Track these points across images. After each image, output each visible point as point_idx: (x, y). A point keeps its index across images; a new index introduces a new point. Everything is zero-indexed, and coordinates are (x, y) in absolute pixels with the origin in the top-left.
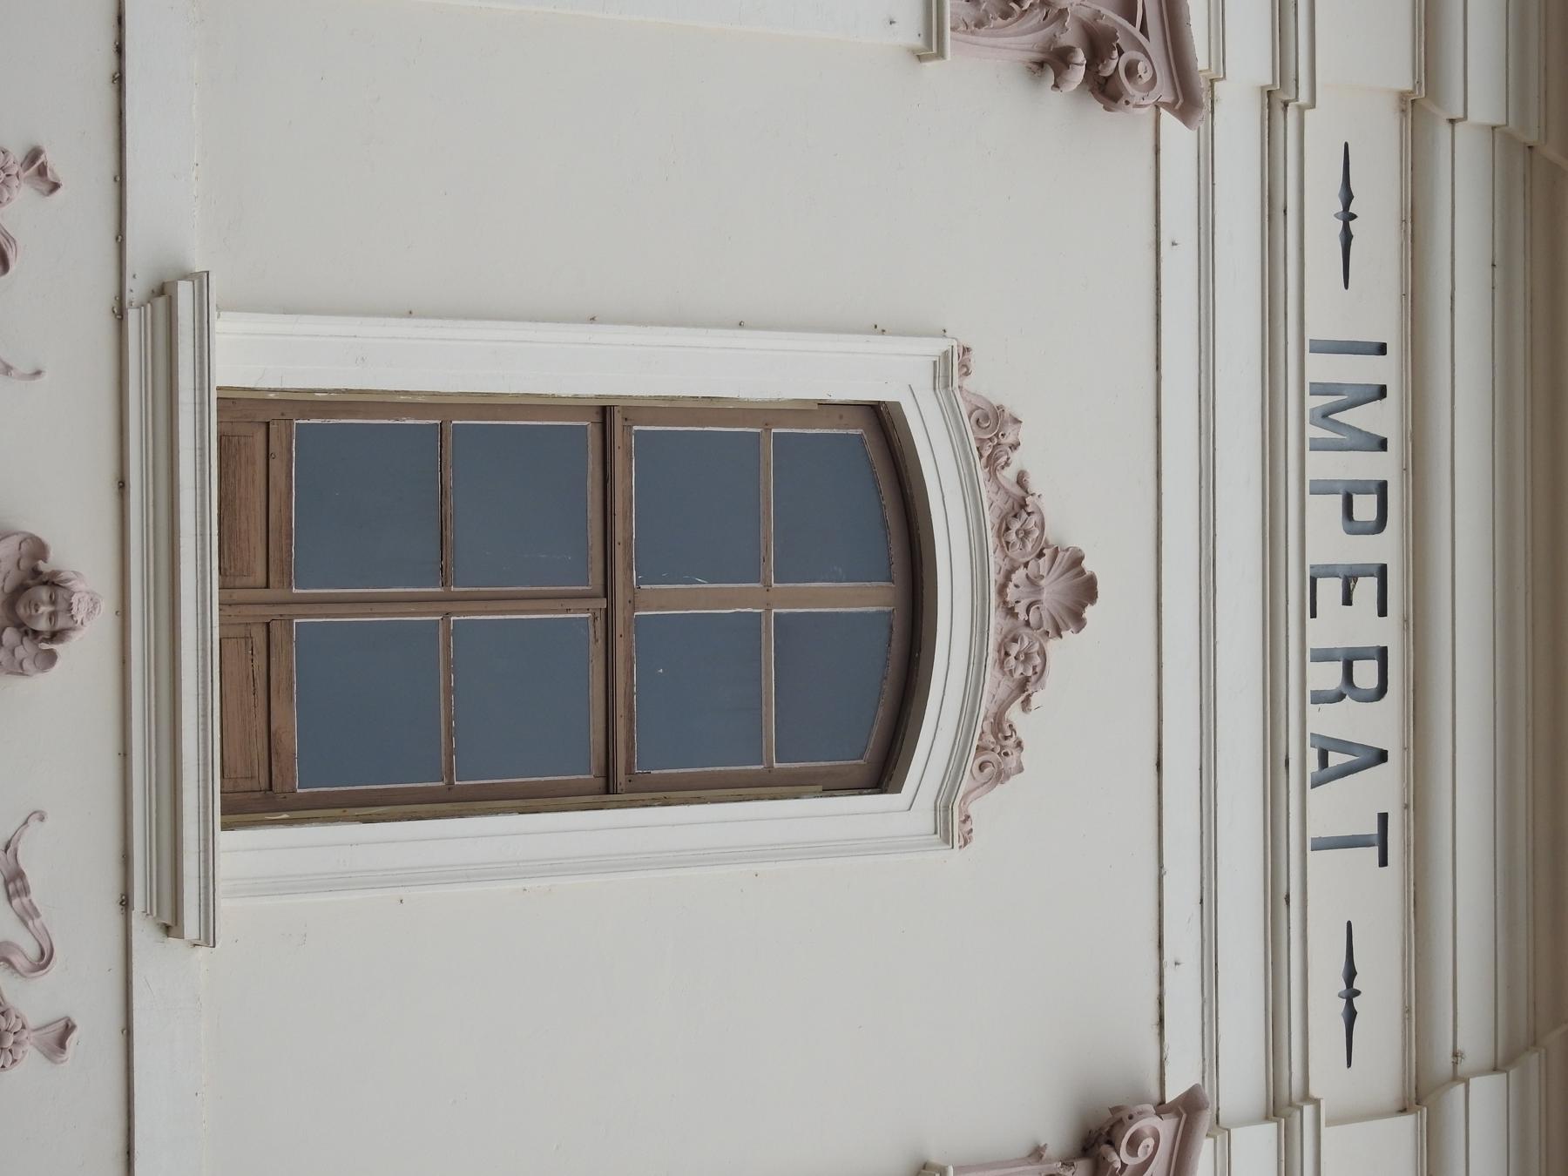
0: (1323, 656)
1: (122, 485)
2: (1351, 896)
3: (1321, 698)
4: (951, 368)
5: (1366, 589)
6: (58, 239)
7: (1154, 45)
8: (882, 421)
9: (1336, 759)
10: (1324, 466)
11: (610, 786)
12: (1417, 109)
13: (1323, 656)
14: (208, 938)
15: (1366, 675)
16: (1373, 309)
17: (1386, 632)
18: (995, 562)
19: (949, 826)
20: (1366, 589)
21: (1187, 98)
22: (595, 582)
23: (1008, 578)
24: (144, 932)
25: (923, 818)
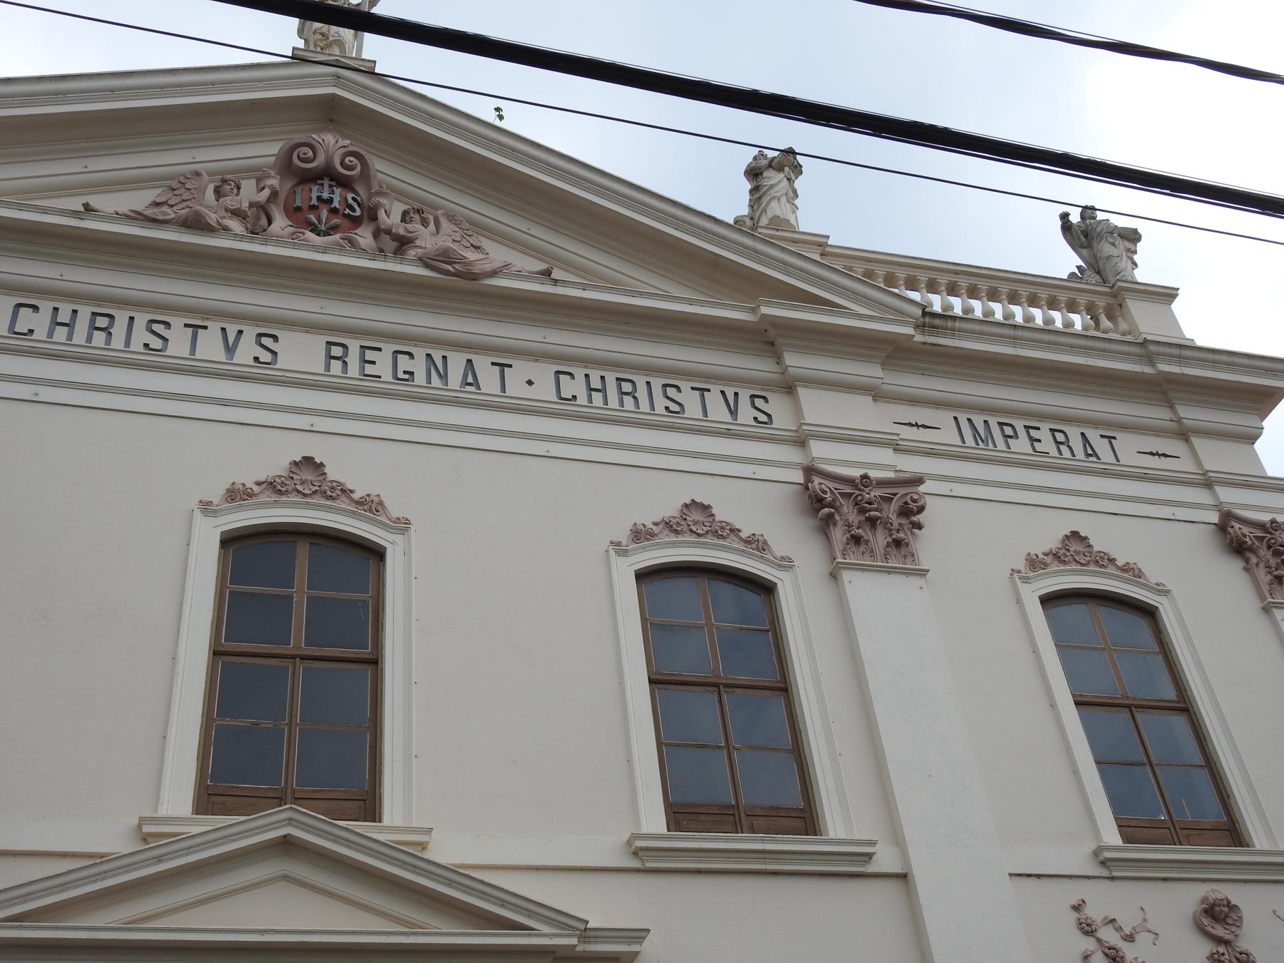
0: (328, 368)
1: (1165, 879)
2: (1130, 449)
3: (108, 342)
4: (207, 508)
5: (370, 355)
6: (1106, 901)
7: (901, 491)
8: (229, 541)
9: (470, 380)
10: (353, 370)
11: (375, 662)
12: (878, 395)
13: (328, 368)
14: (872, 843)
15: (336, 351)
16: (944, 418)
17: (389, 348)
18: (1075, 567)
19: (402, 526)
20: (370, 355)
21: (919, 481)
22: (288, 664)
23: (298, 491)
24: (872, 868)
25: (398, 538)
